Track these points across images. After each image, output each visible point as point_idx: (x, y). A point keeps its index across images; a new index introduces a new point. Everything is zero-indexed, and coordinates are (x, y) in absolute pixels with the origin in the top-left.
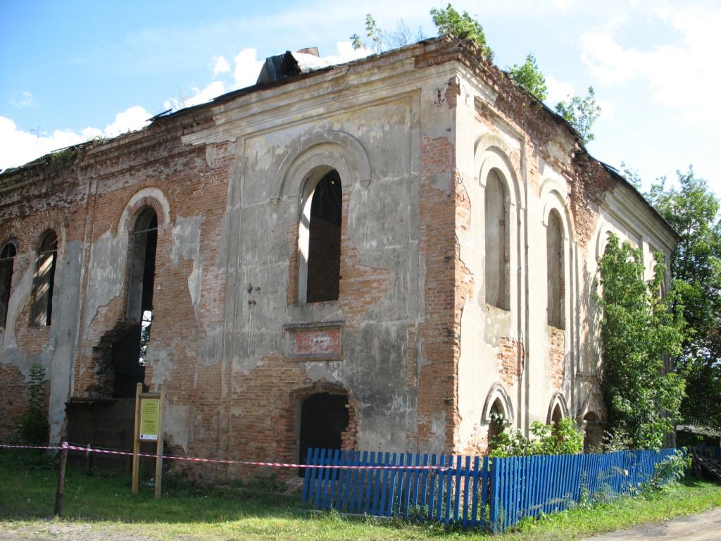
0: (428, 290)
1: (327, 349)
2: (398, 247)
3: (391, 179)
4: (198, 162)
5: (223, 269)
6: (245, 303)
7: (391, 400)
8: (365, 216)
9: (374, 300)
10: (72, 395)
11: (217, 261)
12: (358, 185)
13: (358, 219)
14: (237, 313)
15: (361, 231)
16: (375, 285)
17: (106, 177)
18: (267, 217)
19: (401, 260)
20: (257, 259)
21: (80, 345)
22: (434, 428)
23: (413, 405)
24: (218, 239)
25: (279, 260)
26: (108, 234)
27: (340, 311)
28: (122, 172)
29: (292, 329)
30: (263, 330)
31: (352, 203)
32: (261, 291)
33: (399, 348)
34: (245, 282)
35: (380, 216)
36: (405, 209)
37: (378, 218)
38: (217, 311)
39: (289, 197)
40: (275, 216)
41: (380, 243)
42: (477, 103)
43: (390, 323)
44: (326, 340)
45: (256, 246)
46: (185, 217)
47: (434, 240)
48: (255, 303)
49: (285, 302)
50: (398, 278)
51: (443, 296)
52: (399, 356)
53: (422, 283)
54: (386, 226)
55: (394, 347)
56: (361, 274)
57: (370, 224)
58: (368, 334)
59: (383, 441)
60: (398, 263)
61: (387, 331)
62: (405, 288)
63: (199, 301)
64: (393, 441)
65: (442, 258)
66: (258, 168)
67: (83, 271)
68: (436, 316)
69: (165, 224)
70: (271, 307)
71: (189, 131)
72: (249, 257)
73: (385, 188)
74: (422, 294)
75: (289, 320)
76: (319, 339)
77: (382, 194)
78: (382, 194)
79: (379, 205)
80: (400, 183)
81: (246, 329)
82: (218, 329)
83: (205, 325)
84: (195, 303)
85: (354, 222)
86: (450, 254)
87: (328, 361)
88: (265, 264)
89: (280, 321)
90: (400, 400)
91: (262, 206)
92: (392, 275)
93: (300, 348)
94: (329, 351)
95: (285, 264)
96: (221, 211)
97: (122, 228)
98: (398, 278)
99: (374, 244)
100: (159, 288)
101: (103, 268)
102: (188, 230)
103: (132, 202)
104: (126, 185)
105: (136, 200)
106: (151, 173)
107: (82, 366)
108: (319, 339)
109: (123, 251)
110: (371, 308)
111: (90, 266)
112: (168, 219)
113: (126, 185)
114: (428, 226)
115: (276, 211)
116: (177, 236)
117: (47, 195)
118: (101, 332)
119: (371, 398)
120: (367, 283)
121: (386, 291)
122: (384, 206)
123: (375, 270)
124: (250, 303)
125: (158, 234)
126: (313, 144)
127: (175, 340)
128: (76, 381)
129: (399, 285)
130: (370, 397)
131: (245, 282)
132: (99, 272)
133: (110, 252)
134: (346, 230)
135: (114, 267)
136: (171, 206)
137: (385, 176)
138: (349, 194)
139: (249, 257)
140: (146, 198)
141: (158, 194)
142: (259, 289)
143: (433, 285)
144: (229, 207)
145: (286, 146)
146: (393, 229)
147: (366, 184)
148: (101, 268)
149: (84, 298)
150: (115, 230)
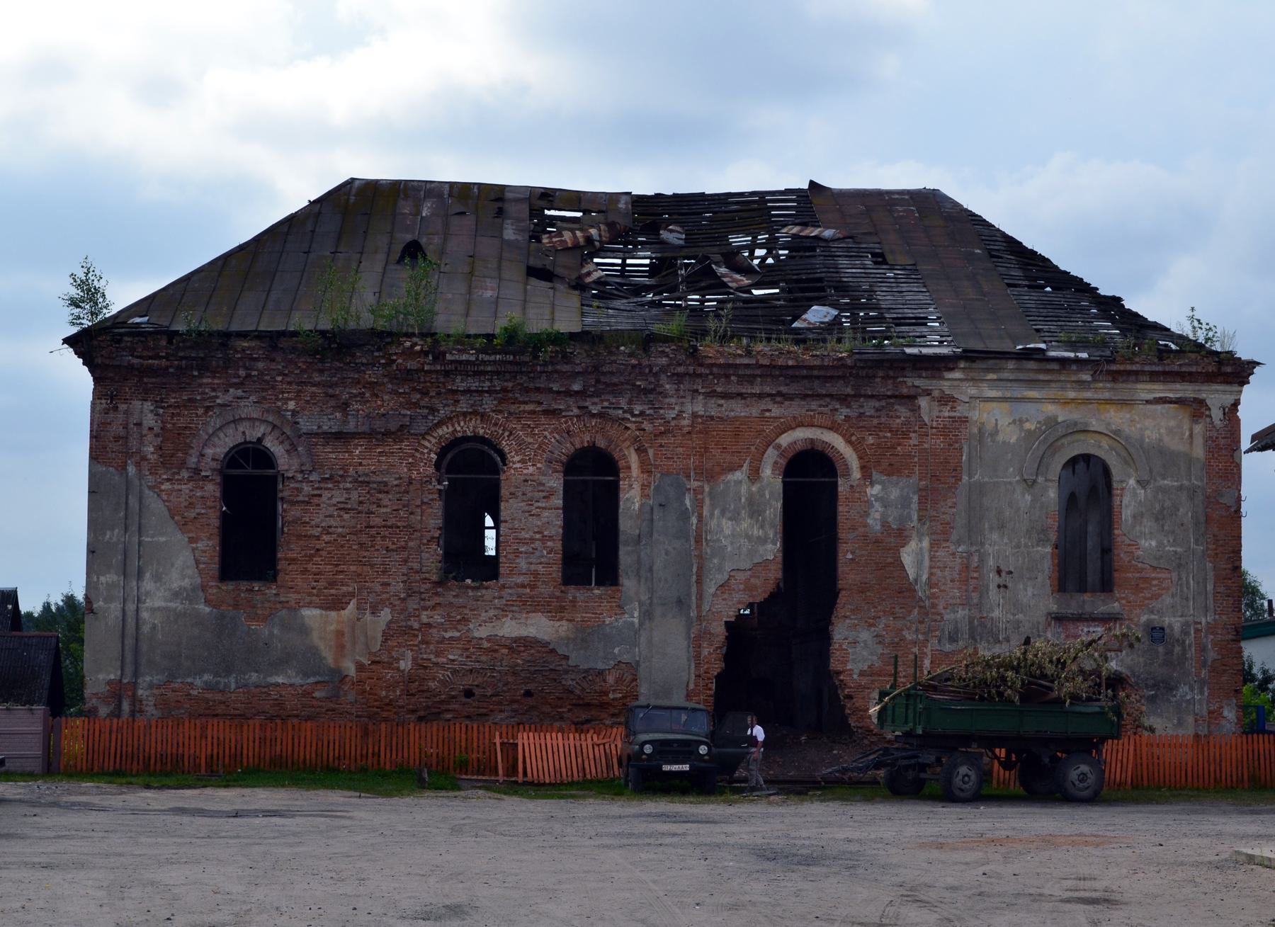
0: (1216, 593)
2: (1179, 550)
4: (903, 411)
6: (993, 586)
7: (1176, 688)
8: (1142, 515)
9: (1156, 597)
11: (954, 537)
12: (1132, 482)
13: (1134, 517)
14: (982, 590)
15: (1138, 528)
16: (1155, 582)
17: (726, 396)
19: (1183, 562)
20: (1006, 540)
21: (699, 617)
22: (1226, 713)
23: (1202, 693)
27: (1116, 604)
28: (760, 396)
29: (1059, 619)
30: (1020, 616)
31: (1126, 500)
32: (1015, 575)
33: (1184, 642)
35: (1159, 517)
37: (1157, 519)
38: (957, 593)
39: (1046, 480)
40: (1028, 498)
41: (1160, 544)
46: (888, 475)
48: (1006, 587)
49: (1049, 590)
50: (1180, 579)
52: (1184, 650)
53: (1210, 587)
55: (1178, 641)
57: (1148, 524)
59: (1170, 725)
62: (1188, 588)
63: (925, 577)
64: (1180, 724)
67: (694, 520)
70: (1030, 593)
72: (995, 536)
73: (1164, 490)
74: (1210, 596)
75: (1054, 608)
76: (1091, 629)
77: (1160, 496)
78: (1160, 496)
79: (1157, 506)
80: (1181, 488)
81: (996, 613)
82: (961, 613)
83: (940, 607)
85: (1130, 520)
86: (1236, 564)
88: (1018, 546)
90: (1186, 688)
92: (1174, 575)
95: (150, 420)
96: (953, 480)
97: (767, 472)
98: (1180, 579)
99: (1154, 543)
101: (735, 518)
102: (894, 494)
103: (785, 440)
106: (813, 407)
108: (1091, 629)
109: (774, 503)
110: (1153, 604)
111: (706, 512)
112: (856, 474)
116: (872, 502)
117: (582, 394)
119: (1155, 686)
120: (1145, 580)
121: (1168, 589)
122: (1163, 509)
123: (1155, 568)
124: (999, 586)
125: (840, 489)
127: (884, 620)
130: (1154, 685)
131: (991, 562)
132: (727, 526)
134: (776, 463)
135: (757, 521)
136: (860, 458)
138: (1122, 489)
142: (1010, 573)
143: (1221, 589)
144: (965, 478)
145: (1039, 422)
146: (1173, 532)
147: (1142, 483)
148: (730, 519)
149: (700, 557)
150: (755, 475)
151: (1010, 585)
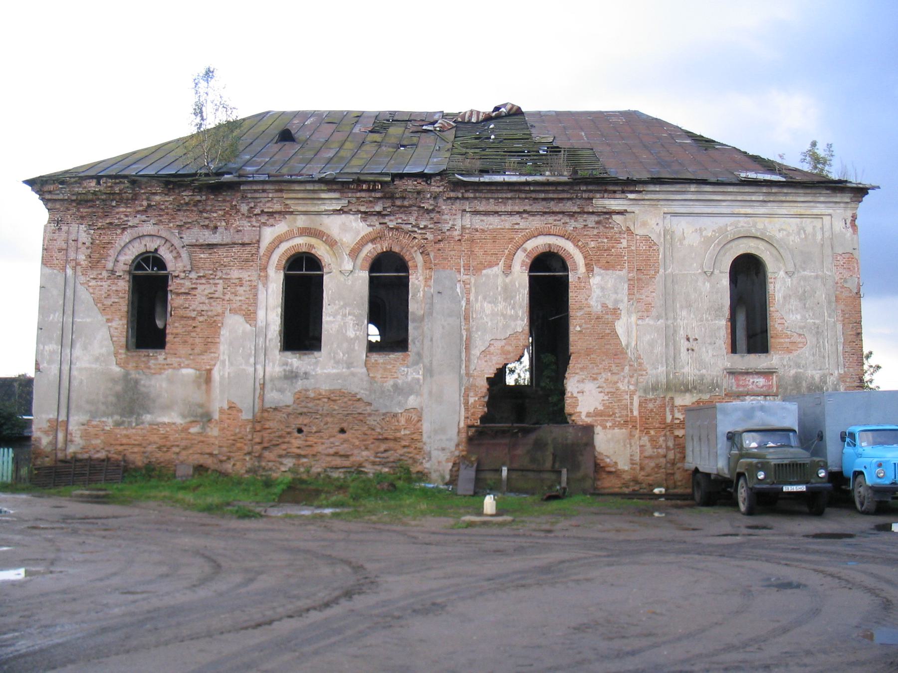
0: (845, 352)
1: (762, 387)
2: (817, 321)
3: (809, 274)
5: (661, 321)
10: (28, 484)
15: (787, 306)
18: (700, 284)
20: (692, 316)
24: (654, 292)
25: (715, 319)
26: (497, 270)
28: (511, 214)
31: (778, 286)
33: (822, 388)
34: (682, 332)
35: (803, 298)
36: (821, 295)
37: (800, 300)
41: (804, 317)
42: (50, 205)
43: (814, 372)
44: (761, 381)
45: (690, 306)
47: (846, 321)
51: (855, 357)
53: (840, 348)
54: (807, 306)
55: (818, 387)
56: (787, 337)
57: (794, 303)
58: (797, 379)
60: (817, 333)
61: (813, 377)
65: (854, 333)
66: (686, 242)
67: (464, 303)
68: (851, 370)
69: (579, 272)
71: (611, 195)
72: (684, 313)
73: (805, 278)
76: (756, 380)
77: (802, 283)
80: (817, 277)
81: (686, 370)
84: (627, 346)
86: (859, 331)
87: (766, 396)
89: (721, 365)
91: (694, 274)
93: (738, 386)
94: (764, 389)
99: (799, 317)
100: (578, 329)
101: (494, 302)
103: (530, 245)
104: (517, 227)
105: (538, 244)
107: (472, 394)
108: (756, 380)
112: (582, 269)
113: (517, 227)
114: (843, 311)
115: (709, 281)
118: (497, 364)
126: (729, 239)
128: (467, 410)
129: (819, 347)
132: (488, 307)
133: (502, 288)
136: (585, 258)
137: (804, 270)
139: (684, 313)
140: (549, 245)
141: (568, 247)
145: (714, 231)
150: (509, 267)
151: (696, 348)
